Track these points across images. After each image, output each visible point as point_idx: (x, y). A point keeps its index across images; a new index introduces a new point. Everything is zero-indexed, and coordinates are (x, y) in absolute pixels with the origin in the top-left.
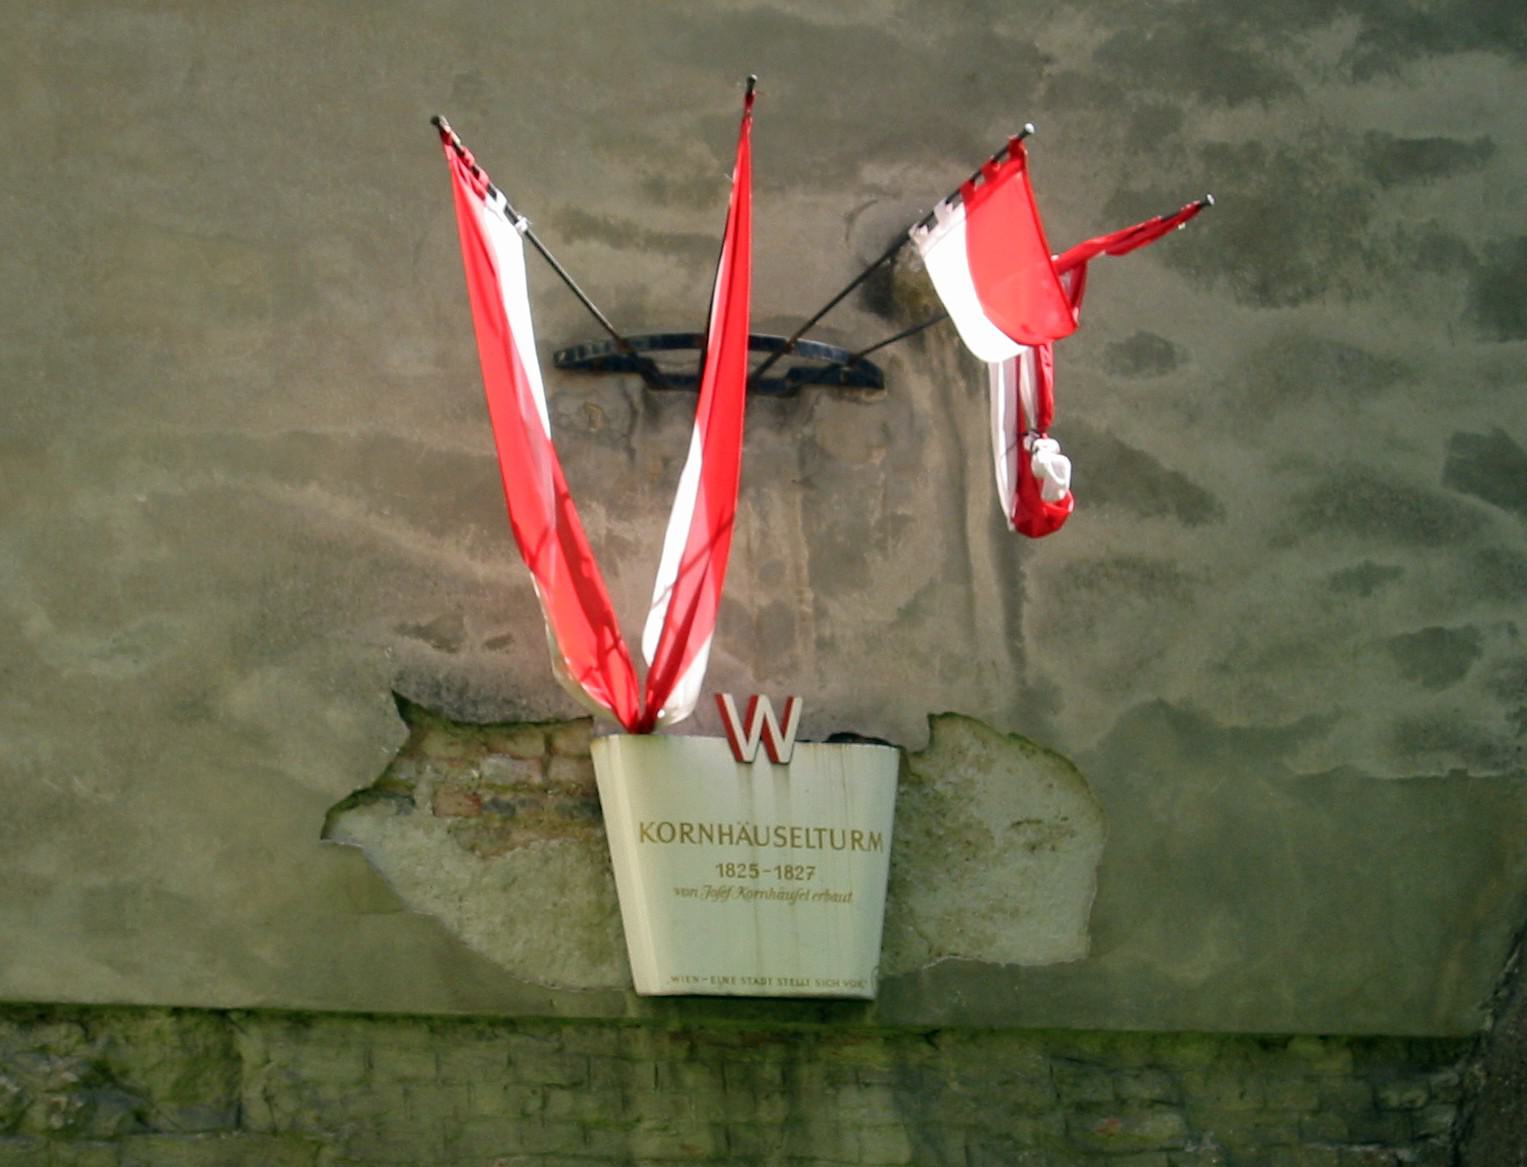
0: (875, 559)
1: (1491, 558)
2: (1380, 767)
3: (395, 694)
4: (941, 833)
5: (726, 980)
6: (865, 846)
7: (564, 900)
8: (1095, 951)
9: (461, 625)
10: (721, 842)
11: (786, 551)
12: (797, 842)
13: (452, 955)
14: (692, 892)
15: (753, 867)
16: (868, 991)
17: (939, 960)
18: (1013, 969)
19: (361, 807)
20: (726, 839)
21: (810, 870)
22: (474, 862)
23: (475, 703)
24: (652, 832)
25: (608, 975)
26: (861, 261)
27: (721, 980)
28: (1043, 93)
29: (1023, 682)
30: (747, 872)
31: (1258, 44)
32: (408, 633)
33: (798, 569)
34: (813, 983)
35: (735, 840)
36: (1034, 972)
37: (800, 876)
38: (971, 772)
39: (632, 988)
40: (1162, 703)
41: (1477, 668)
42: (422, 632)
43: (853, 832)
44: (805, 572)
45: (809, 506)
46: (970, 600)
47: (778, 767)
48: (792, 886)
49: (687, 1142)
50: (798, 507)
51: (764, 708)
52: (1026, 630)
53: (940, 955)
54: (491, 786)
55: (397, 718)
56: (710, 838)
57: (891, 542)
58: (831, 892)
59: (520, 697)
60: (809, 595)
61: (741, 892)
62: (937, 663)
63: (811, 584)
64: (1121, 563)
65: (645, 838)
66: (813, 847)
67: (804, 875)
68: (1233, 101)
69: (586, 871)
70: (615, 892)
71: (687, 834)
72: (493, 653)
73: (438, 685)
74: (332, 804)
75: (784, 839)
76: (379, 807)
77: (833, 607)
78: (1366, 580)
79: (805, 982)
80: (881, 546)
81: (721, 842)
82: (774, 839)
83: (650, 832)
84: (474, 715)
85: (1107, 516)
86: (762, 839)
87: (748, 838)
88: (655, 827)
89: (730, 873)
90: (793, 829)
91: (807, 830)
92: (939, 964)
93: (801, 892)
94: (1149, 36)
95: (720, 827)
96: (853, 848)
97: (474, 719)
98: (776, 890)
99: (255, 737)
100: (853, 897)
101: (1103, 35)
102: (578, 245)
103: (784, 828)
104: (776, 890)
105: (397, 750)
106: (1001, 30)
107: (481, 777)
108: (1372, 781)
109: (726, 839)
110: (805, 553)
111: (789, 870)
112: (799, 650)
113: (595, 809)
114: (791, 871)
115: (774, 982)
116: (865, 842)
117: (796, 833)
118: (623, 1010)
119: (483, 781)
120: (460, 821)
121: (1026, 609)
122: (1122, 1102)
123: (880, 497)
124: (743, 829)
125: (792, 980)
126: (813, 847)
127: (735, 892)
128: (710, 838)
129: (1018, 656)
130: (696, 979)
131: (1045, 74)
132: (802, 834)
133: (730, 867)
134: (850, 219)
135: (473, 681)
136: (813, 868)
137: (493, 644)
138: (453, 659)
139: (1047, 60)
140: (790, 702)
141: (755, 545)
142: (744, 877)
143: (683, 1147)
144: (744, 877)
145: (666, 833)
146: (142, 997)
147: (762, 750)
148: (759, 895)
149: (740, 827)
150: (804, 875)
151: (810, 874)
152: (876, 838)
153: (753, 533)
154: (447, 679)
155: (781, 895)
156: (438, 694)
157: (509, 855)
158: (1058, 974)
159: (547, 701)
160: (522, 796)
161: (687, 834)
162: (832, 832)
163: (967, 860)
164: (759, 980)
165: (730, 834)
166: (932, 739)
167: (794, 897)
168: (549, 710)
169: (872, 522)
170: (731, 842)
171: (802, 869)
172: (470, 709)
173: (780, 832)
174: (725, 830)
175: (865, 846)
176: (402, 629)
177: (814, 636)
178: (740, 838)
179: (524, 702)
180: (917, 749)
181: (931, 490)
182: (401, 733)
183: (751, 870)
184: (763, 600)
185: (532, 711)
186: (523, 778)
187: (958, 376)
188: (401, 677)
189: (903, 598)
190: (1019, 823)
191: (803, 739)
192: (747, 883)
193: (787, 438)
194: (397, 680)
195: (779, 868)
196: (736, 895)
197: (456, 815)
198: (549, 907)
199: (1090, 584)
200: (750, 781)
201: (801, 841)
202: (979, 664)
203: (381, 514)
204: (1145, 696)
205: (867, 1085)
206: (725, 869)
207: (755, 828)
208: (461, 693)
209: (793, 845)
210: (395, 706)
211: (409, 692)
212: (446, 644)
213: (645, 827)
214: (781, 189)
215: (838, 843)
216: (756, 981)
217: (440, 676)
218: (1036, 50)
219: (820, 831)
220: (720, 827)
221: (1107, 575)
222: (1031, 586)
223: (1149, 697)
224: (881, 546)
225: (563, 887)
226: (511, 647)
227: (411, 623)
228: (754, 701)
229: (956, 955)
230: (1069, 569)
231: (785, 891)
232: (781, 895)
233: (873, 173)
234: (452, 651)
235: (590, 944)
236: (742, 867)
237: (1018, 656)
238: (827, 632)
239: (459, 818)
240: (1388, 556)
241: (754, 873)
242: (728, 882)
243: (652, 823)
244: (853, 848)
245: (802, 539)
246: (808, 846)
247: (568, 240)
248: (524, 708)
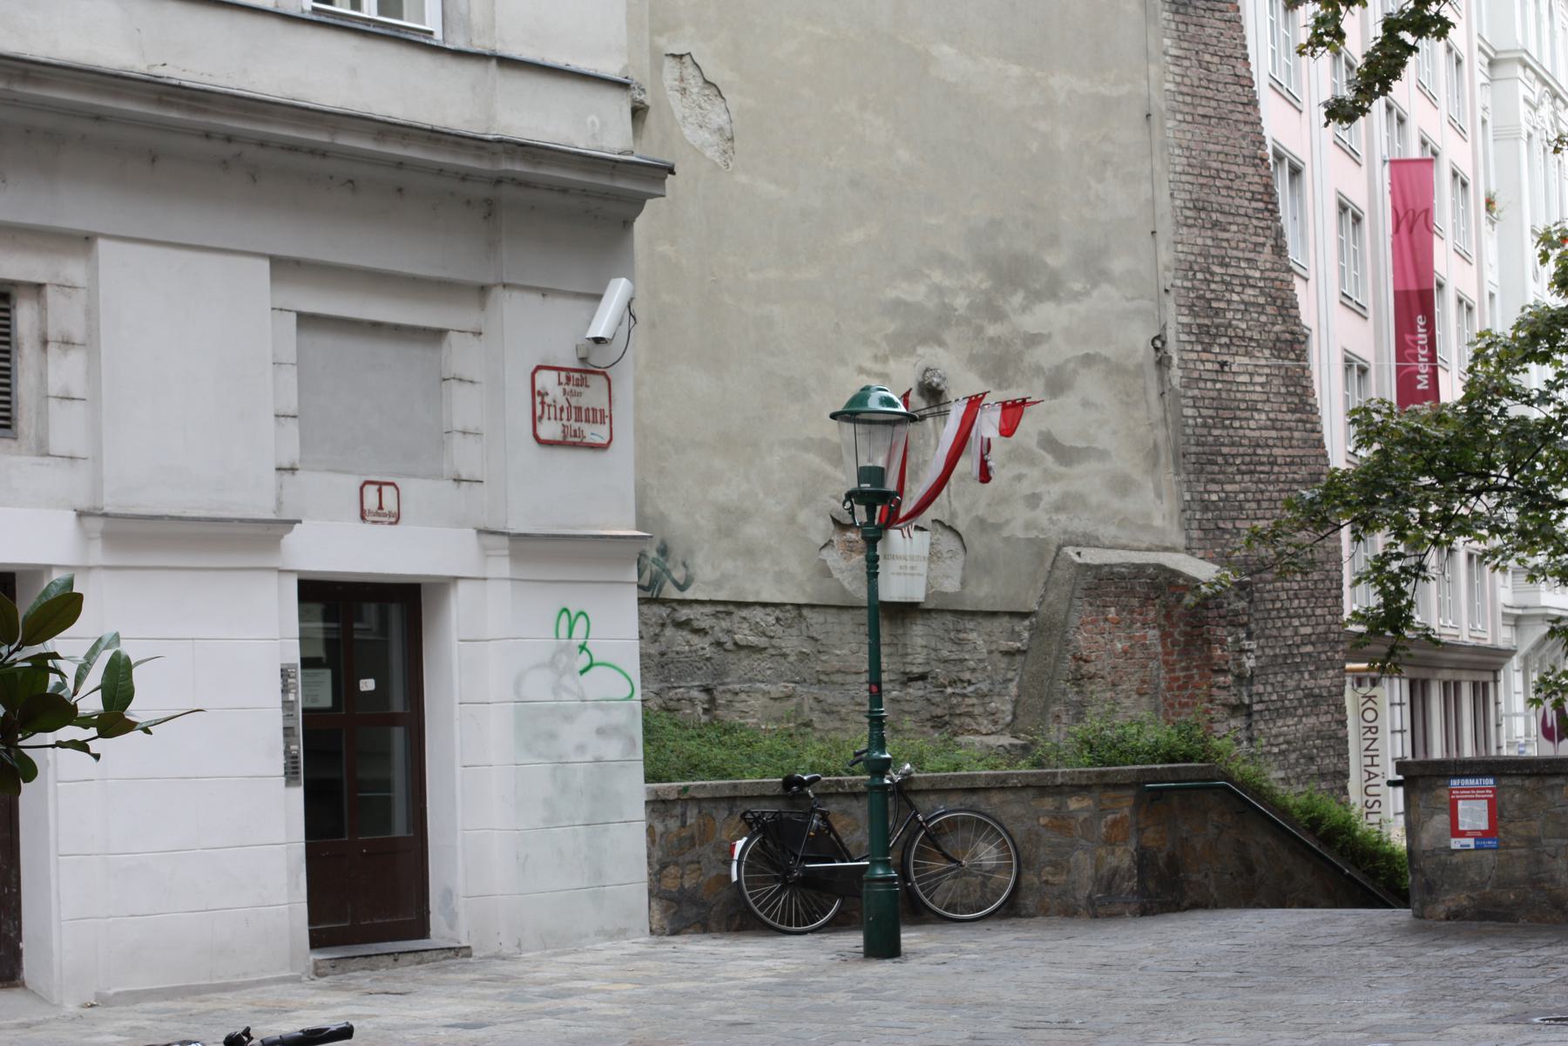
1: (1045, 470)
2: (1021, 534)
8: (962, 588)
13: (844, 591)
20: (1368, 761)
22: (845, 562)
31: (1001, 302)
35: (1368, 769)
41: (1042, 504)
52: (952, 495)
68: (995, 322)
78: (1019, 478)
82: (1372, 800)
87: (1370, 779)
99: (804, 528)
106: (946, 300)
108: (1019, 539)
109: (1368, 761)
122: (965, 629)
124: (1376, 776)
134: (915, 365)
139: (956, 310)
146: (786, 601)
158: (956, 594)
165: (1372, 765)
178: (1370, 773)
204: (974, 514)
211: (834, 515)
233: (920, 350)
237: (950, 502)
240: (1025, 470)
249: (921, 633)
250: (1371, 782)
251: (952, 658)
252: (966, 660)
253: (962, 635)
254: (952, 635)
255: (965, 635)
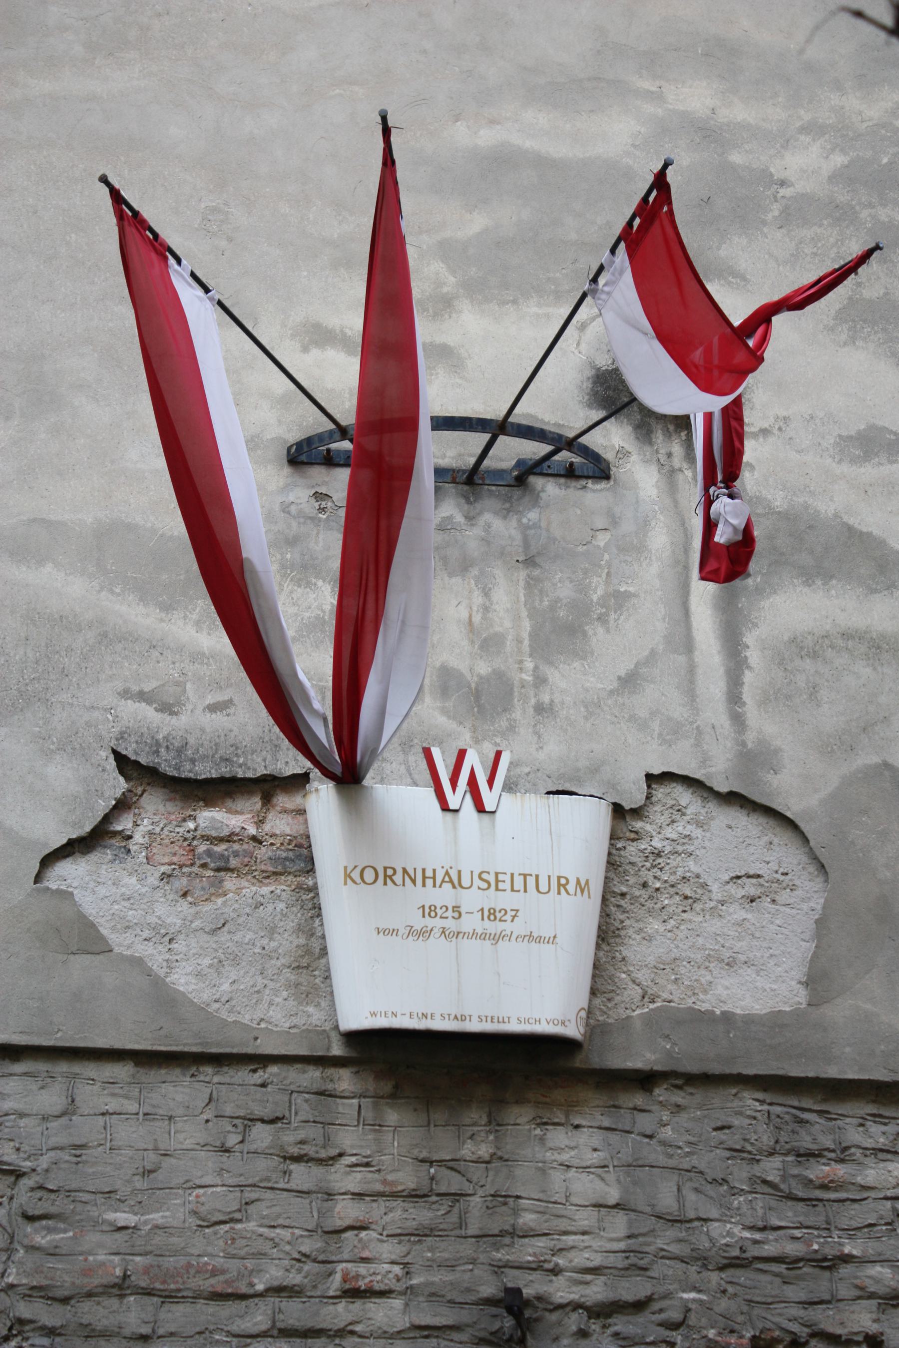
0: (597, 635)
3: (114, 752)
4: (658, 885)
5: (425, 1016)
6: (572, 891)
7: (273, 944)
9: (184, 691)
10: (424, 885)
11: (508, 624)
12: (501, 886)
14: (394, 932)
15: (456, 908)
16: (573, 1031)
17: (652, 1006)
18: (727, 1018)
19: (77, 854)
21: (513, 913)
23: (193, 761)
24: (356, 875)
25: (315, 1016)
26: (592, 365)
27: (420, 1015)
28: (776, 213)
29: (744, 744)
30: (450, 913)
32: (131, 698)
33: (519, 641)
34: (514, 1021)
35: (438, 884)
36: (750, 1020)
37: (503, 918)
38: (690, 829)
39: (337, 1027)
40: (886, 765)
42: (143, 697)
43: (559, 878)
44: (526, 642)
45: (532, 584)
46: (691, 669)
47: (484, 816)
48: (492, 927)
49: (390, 1178)
50: (522, 583)
51: (472, 760)
52: (747, 694)
53: (653, 1002)
54: (206, 838)
55: (116, 773)
56: (414, 881)
57: (613, 616)
58: (535, 935)
59: (237, 755)
60: (529, 665)
61: (443, 932)
62: (656, 726)
63: (531, 655)
64: (846, 635)
65: (348, 880)
66: (519, 891)
67: (508, 917)
69: (295, 917)
70: (323, 937)
71: (390, 877)
72: (214, 716)
73: (158, 744)
74: (47, 852)
75: (480, 878)
76: (95, 857)
77: (553, 675)
79: (506, 1020)
80: (602, 619)
81: (424, 885)
83: (352, 875)
84: (190, 771)
85: (833, 592)
86: (466, 882)
87: (451, 881)
88: (358, 870)
89: (433, 914)
90: (497, 874)
91: (512, 875)
92: (652, 1010)
93: (503, 934)
94: (885, 160)
95: (424, 870)
96: (559, 893)
97: (191, 775)
98: (479, 931)
100: (557, 940)
101: (839, 160)
102: (315, 353)
103: (488, 873)
104: (479, 931)
105: (114, 802)
106: (736, 158)
107: (196, 830)
109: (429, 882)
110: (527, 625)
111: (492, 912)
112: (517, 714)
113: (310, 862)
114: (494, 914)
115: (475, 1019)
116: (571, 888)
117: (501, 877)
118: (329, 1048)
119: (198, 833)
120: (174, 869)
121: (748, 677)
123: (604, 576)
124: (447, 873)
125: (492, 1018)
126: (519, 891)
127: (437, 932)
128: (414, 881)
129: (738, 720)
130: (394, 1015)
131: (779, 195)
132: (507, 878)
133: (433, 909)
135: (192, 741)
136: (517, 911)
137: (213, 708)
138: (174, 720)
139: (783, 183)
140: (498, 754)
141: (477, 619)
142: (447, 918)
143: (384, 1182)
144: (447, 918)
145: (369, 875)
147: (469, 798)
148: (461, 935)
149: (444, 871)
150: (508, 917)
151: (514, 917)
152: (583, 883)
153: (475, 608)
154: (166, 738)
155: (484, 936)
156: (157, 752)
157: (220, 901)
159: (264, 760)
160: (236, 846)
161: (390, 877)
162: (537, 876)
163: (684, 911)
164: (459, 1017)
165: (434, 878)
166: (648, 797)
167: (496, 938)
168: (265, 767)
169: (595, 598)
170: (434, 886)
171: (506, 912)
172: (188, 766)
173: (484, 876)
174: (429, 873)
175: (572, 891)
176: (126, 694)
177: (533, 701)
178: (443, 881)
179: (241, 760)
180: (634, 806)
181: (654, 569)
182: (119, 785)
183: (453, 911)
184: (483, 668)
185: (249, 768)
186: (237, 830)
187: (685, 465)
188: (121, 737)
189: (624, 667)
190: (738, 877)
191: (509, 787)
192: (450, 924)
193: (514, 523)
194: (117, 740)
195: (482, 910)
196: (438, 935)
197: (170, 864)
198: (257, 950)
199: (814, 655)
200: (455, 829)
201: (507, 885)
202: (698, 728)
203: (112, 592)
205: (577, 1127)
206: (427, 910)
207: (459, 872)
208: (180, 751)
209: (497, 889)
210: (114, 763)
211: (129, 751)
212: (167, 708)
213: (348, 871)
214: (515, 302)
215: (543, 887)
216: (456, 1017)
217: (160, 736)
218: (772, 175)
219: (525, 876)
220: (424, 870)
221: (832, 647)
222: (753, 656)
223: (875, 759)
224: (602, 619)
225: (272, 931)
226: (232, 710)
227: (135, 688)
228: (462, 754)
229: (670, 1002)
230: (793, 640)
231: (488, 932)
232: (484, 936)
234: (172, 713)
235: (297, 985)
236: (444, 909)
237: (738, 720)
238: (546, 698)
239: (173, 867)
241: (456, 915)
242: (429, 922)
243: (356, 867)
244: (559, 893)
245: (524, 613)
246: (512, 890)
247: (305, 349)
248: (240, 766)
249: (594, 1158)
250: (456, 882)
251: (769, 1250)
252: (847, 1259)
253: (819, 1171)
254: (771, 1168)
255: (841, 1171)
